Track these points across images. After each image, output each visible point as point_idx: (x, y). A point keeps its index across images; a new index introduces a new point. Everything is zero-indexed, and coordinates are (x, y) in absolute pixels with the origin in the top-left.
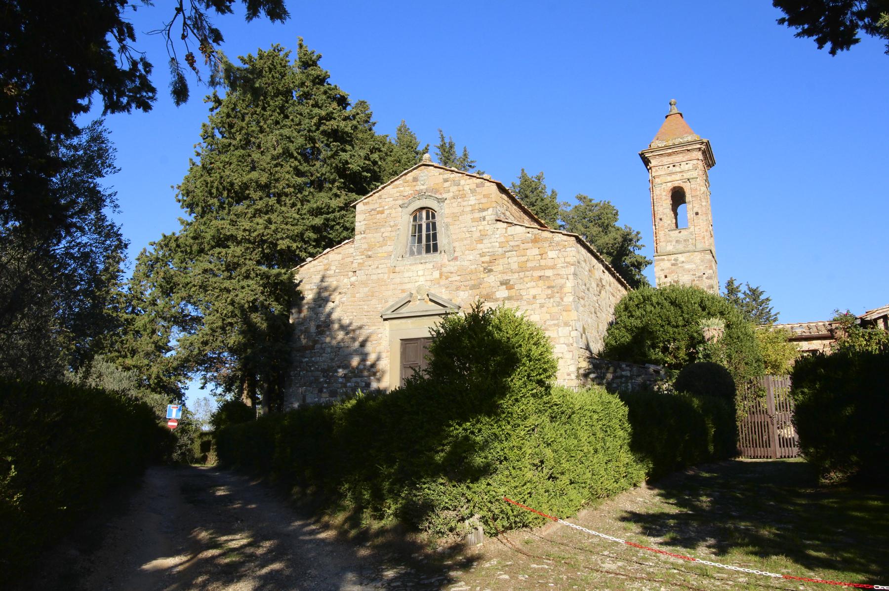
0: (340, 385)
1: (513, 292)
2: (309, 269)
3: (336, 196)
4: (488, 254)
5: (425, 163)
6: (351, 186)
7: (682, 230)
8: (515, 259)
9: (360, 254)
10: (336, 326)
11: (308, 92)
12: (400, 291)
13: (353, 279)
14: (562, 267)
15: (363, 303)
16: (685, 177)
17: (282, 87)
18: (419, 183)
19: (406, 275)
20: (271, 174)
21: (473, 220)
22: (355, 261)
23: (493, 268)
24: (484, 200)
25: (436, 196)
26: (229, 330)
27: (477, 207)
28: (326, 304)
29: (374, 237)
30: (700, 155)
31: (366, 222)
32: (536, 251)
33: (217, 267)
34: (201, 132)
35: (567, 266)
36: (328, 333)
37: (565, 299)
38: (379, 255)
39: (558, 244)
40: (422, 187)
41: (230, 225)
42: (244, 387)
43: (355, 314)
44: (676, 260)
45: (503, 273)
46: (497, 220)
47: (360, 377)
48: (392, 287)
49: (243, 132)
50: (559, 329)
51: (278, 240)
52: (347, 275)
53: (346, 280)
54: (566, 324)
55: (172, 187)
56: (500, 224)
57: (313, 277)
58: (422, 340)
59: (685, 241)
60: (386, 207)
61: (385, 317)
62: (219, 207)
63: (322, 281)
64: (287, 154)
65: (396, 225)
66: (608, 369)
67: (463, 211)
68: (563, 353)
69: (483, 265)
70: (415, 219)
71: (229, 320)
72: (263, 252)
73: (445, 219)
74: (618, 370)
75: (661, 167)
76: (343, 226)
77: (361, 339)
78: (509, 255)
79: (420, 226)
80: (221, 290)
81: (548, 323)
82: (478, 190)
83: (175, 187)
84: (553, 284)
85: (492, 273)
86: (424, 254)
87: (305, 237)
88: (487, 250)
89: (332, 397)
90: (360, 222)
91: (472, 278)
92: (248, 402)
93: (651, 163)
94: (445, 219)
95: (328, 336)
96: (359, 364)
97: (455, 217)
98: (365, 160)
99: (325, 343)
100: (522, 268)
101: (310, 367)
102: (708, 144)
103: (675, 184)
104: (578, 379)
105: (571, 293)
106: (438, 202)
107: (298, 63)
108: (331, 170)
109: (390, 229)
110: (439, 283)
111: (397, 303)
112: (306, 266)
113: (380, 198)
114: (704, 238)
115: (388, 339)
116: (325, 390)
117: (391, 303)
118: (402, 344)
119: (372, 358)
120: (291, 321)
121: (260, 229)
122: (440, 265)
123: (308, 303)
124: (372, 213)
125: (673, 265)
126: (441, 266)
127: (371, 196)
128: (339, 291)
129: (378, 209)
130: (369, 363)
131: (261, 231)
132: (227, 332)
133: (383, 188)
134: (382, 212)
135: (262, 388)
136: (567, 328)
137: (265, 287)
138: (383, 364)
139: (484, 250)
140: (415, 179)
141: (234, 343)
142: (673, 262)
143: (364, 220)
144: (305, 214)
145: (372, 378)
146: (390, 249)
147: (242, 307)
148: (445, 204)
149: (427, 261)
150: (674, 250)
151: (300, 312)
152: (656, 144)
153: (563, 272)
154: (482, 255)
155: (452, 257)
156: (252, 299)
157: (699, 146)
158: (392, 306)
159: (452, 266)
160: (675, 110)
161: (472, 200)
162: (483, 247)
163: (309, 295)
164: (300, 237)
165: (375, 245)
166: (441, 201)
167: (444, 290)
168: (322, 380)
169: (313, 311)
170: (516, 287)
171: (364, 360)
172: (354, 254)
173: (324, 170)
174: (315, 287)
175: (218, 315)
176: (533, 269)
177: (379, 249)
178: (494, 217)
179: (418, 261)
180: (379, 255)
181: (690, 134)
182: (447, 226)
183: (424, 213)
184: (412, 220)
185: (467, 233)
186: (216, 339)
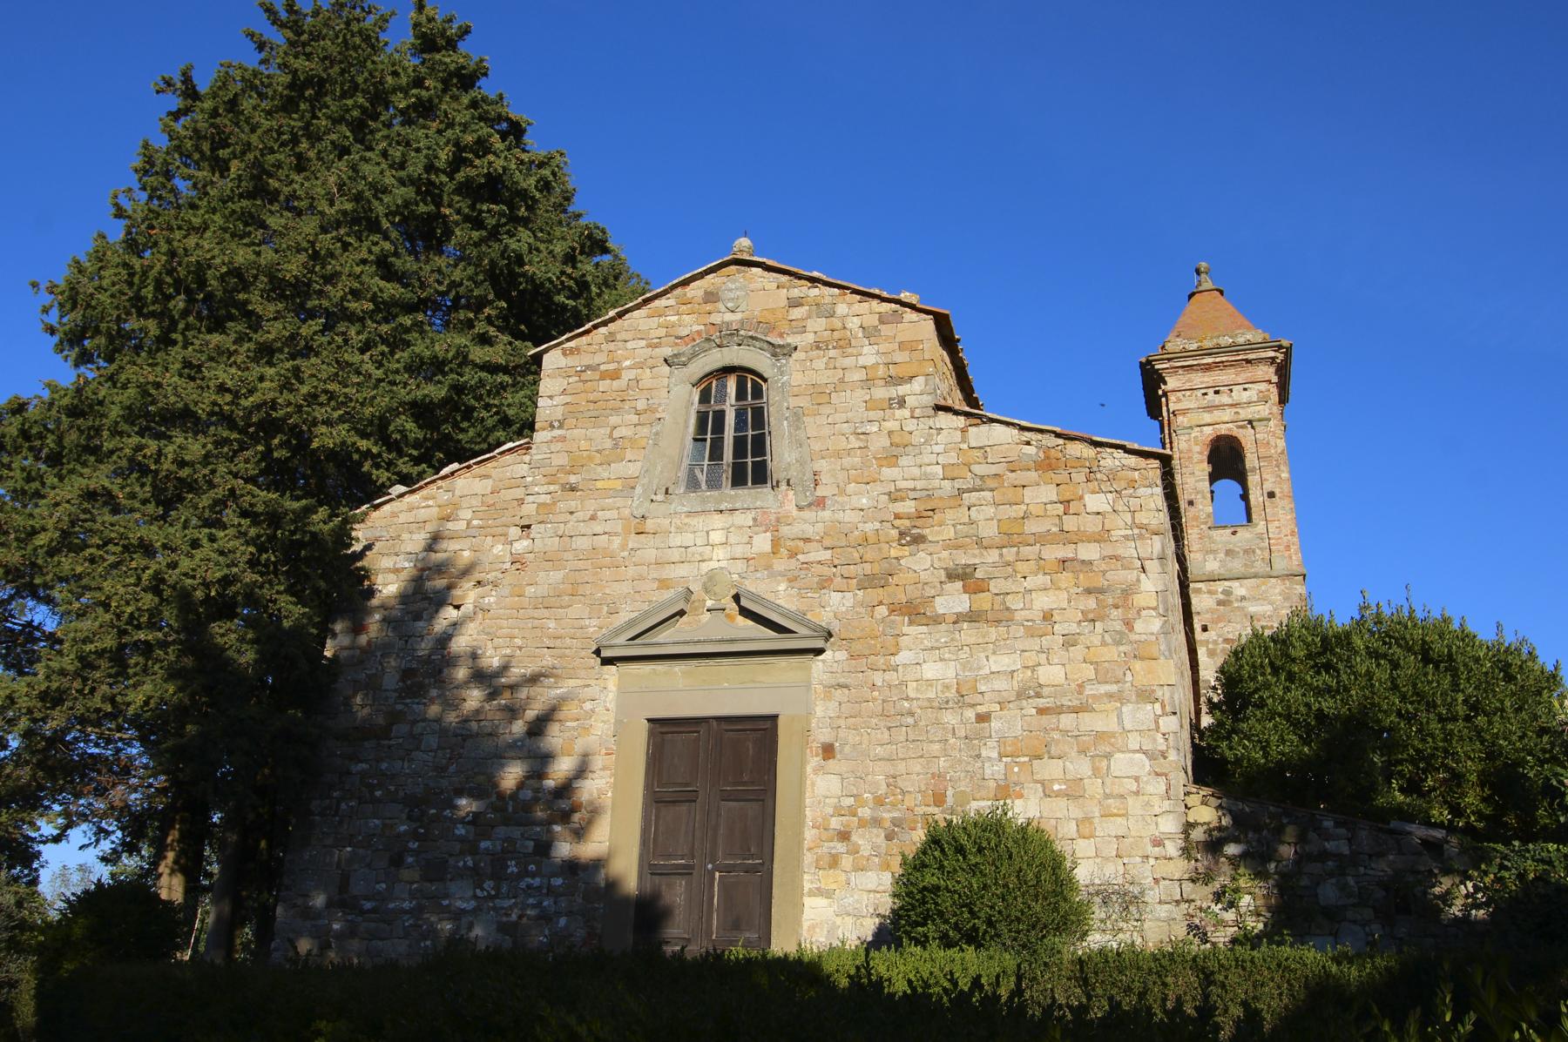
0: (458, 846)
1: (984, 601)
2: (394, 515)
3: (484, 340)
4: (912, 495)
5: (739, 256)
6: (523, 327)
7: (1239, 529)
8: (991, 511)
9: (544, 480)
10: (461, 673)
11: (430, 100)
12: (655, 585)
13: (521, 546)
14: (1126, 537)
15: (546, 613)
16: (1242, 416)
17: (366, 80)
18: (720, 306)
19: (676, 540)
20: (315, 256)
21: (870, 405)
22: (531, 498)
23: (926, 532)
24: (900, 357)
25: (769, 339)
26: (137, 664)
27: (881, 372)
28: (437, 611)
29: (586, 437)
30: (1270, 372)
31: (568, 399)
32: (1049, 493)
33: (128, 490)
34: (138, 162)
35: (1141, 536)
36: (434, 692)
37: (1139, 626)
38: (599, 484)
39: (1112, 477)
40: (729, 317)
41: (181, 375)
42: (169, 840)
43: (518, 642)
44: (1227, 592)
45: (958, 547)
46: (938, 408)
47: (519, 824)
48: (631, 571)
49: (250, 156)
50: (1124, 709)
51: (315, 423)
52: (505, 535)
53: (500, 547)
54: (1146, 696)
55: (35, 285)
56: (945, 419)
57: (405, 536)
58: (715, 723)
59: (1246, 552)
60: (627, 363)
61: (606, 653)
62: (158, 339)
63: (430, 548)
64: (365, 223)
65: (650, 409)
66: (1279, 831)
67: (842, 381)
68: (1137, 779)
69: (897, 522)
70: (705, 397)
71: (142, 635)
72: (267, 455)
73: (790, 399)
74: (1312, 835)
75: (1188, 393)
76: (497, 413)
77: (531, 714)
78: (973, 501)
79: (720, 416)
80: (126, 548)
81: (1090, 690)
82: (886, 330)
83: (42, 287)
84: (1101, 582)
85: (922, 546)
86: (728, 491)
87: (391, 428)
88: (910, 484)
89: (431, 881)
90: (551, 397)
91: (867, 557)
92: (171, 888)
93: (1165, 383)
94: (790, 399)
95: (432, 701)
96: (521, 785)
97: (822, 396)
98: (565, 263)
99: (425, 720)
100: (1011, 537)
101: (372, 788)
102: (1288, 353)
103: (1220, 429)
104: (1189, 858)
105: (1154, 609)
106: (774, 355)
107: (410, 39)
108: (477, 274)
109: (635, 419)
110: (768, 567)
111: (646, 615)
112: (386, 508)
113: (611, 338)
114: (1288, 548)
115: (611, 717)
116: (410, 860)
117: (624, 616)
118: (651, 734)
119: (562, 767)
120: (328, 653)
121: (267, 390)
122: (773, 517)
123: (383, 607)
124: (584, 376)
125: (1220, 603)
126: (778, 520)
127: (587, 332)
128: (477, 576)
129: (603, 367)
130: (550, 783)
131: (271, 395)
132: (131, 671)
133: (620, 315)
134: (615, 375)
135: (221, 847)
136: (1149, 707)
137: (262, 549)
138: (594, 788)
139: (902, 484)
140: (711, 297)
141: (146, 703)
142: (1221, 597)
143: (564, 392)
144: (397, 372)
145: (557, 828)
146: (633, 469)
147: (184, 596)
148: (791, 360)
149: (738, 505)
150: (1222, 571)
151: (358, 628)
152: (1175, 345)
153: (1128, 550)
154: (894, 497)
155: (810, 499)
156: (218, 575)
157: (1272, 354)
158: (631, 623)
159: (808, 524)
160: (1208, 284)
161: (869, 355)
162: (902, 474)
163: (389, 587)
164: (379, 428)
165: (590, 458)
166: (781, 352)
167: (782, 587)
168: (403, 828)
169: (394, 629)
170: (994, 587)
171: (537, 773)
172: (529, 479)
173: (457, 275)
174: (407, 565)
175: (108, 617)
176: (1042, 539)
177: (599, 469)
178: (929, 400)
179: (711, 506)
180: (599, 484)
181: (1249, 329)
182: (797, 417)
183: (731, 384)
184: (697, 399)
185: (852, 438)
186: (93, 690)
